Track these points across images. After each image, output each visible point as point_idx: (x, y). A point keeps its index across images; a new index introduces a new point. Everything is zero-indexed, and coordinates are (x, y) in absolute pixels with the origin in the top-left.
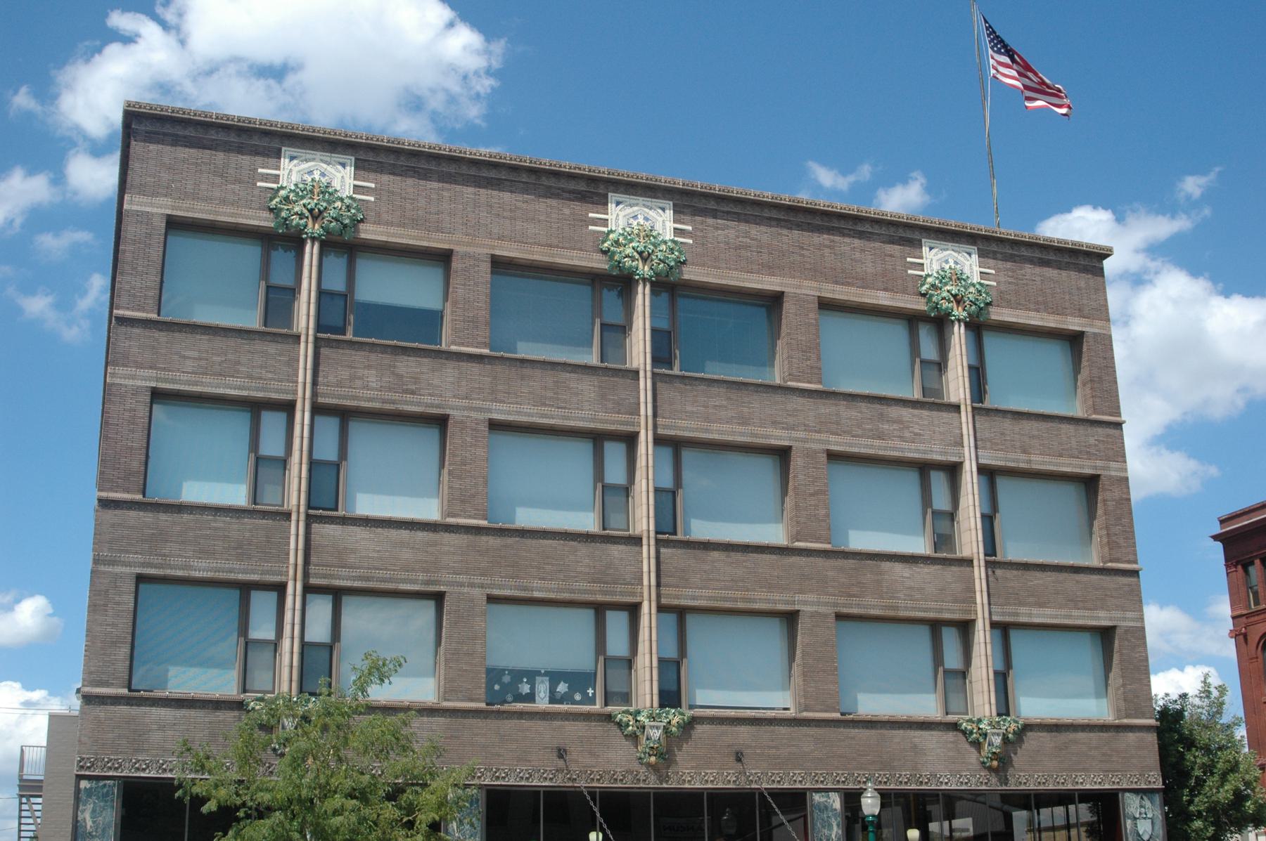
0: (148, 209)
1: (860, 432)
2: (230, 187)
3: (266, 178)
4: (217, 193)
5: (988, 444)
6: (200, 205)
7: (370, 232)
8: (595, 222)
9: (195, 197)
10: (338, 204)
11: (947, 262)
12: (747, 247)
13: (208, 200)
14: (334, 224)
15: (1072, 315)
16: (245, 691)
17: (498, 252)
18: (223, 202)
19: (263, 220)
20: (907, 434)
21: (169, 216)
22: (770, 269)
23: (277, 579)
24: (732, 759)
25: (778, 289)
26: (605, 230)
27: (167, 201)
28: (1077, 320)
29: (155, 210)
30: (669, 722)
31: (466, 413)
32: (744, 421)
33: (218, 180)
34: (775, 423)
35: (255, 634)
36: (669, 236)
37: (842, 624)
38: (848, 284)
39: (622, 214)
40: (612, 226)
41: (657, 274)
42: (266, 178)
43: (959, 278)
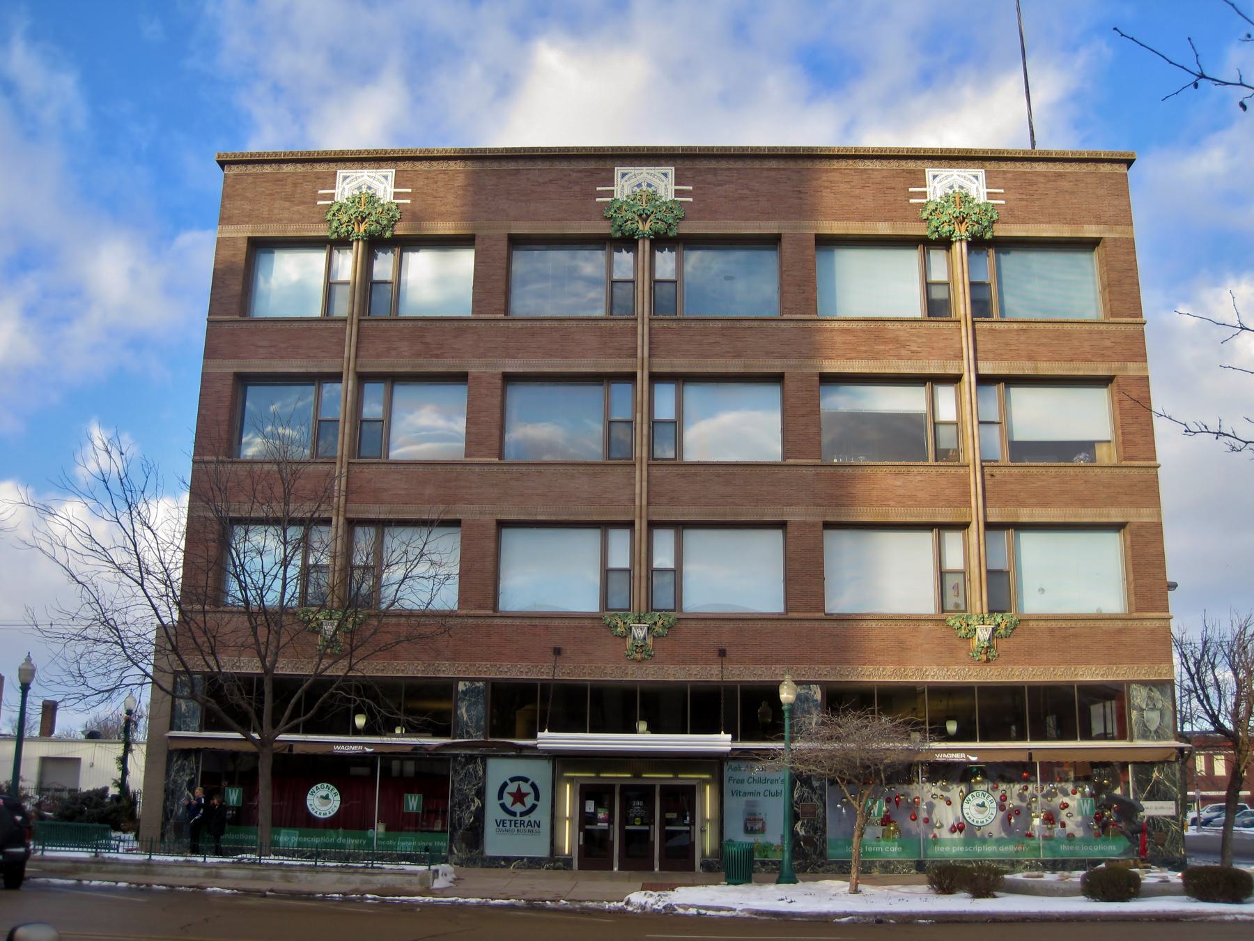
0: (234, 235)
1: (854, 355)
2: (295, 208)
3: (324, 197)
4: (286, 215)
5: (991, 356)
6: (274, 226)
7: (1001, 231)
8: (602, 194)
9: (270, 220)
10: (977, 210)
11: (951, 187)
12: (742, 198)
13: (279, 221)
14: (975, 228)
15: (1090, 223)
16: (943, 611)
17: (513, 232)
18: (291, 221)
19: (602, 228)
20: (903, 352)
21: (249, 238)
22: (766, 215)
23: (629, 518)
24: (551, 652)
25: (775, 232)
26: (924, 201)
27: (250, 227)
28: (1094, 227)
29: (240, 235)
30: (655, 623)
31: (483, 370)
32: (738, 355)
33: (287, 204)
34: (768, 354)
35: (657, 563)
36: (982, 199)
37: (991, 534)
38: (847, 219)
39: (626, 184)
40: (930, 197)
41: (973, 236)
42: (324, 197)
43: (965, 199)
